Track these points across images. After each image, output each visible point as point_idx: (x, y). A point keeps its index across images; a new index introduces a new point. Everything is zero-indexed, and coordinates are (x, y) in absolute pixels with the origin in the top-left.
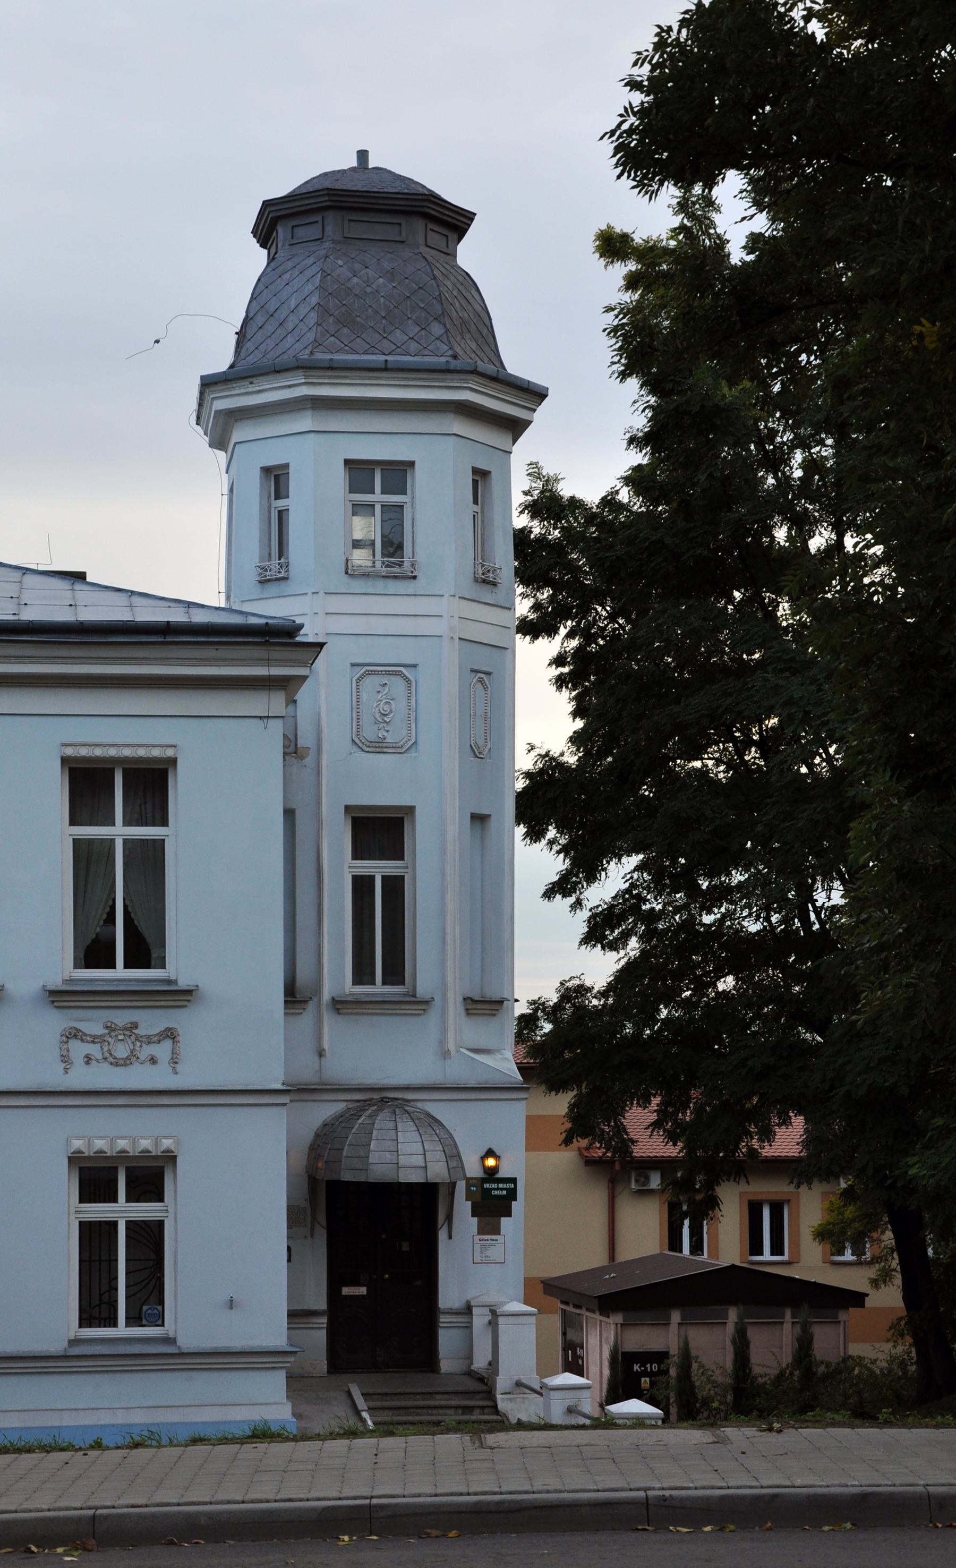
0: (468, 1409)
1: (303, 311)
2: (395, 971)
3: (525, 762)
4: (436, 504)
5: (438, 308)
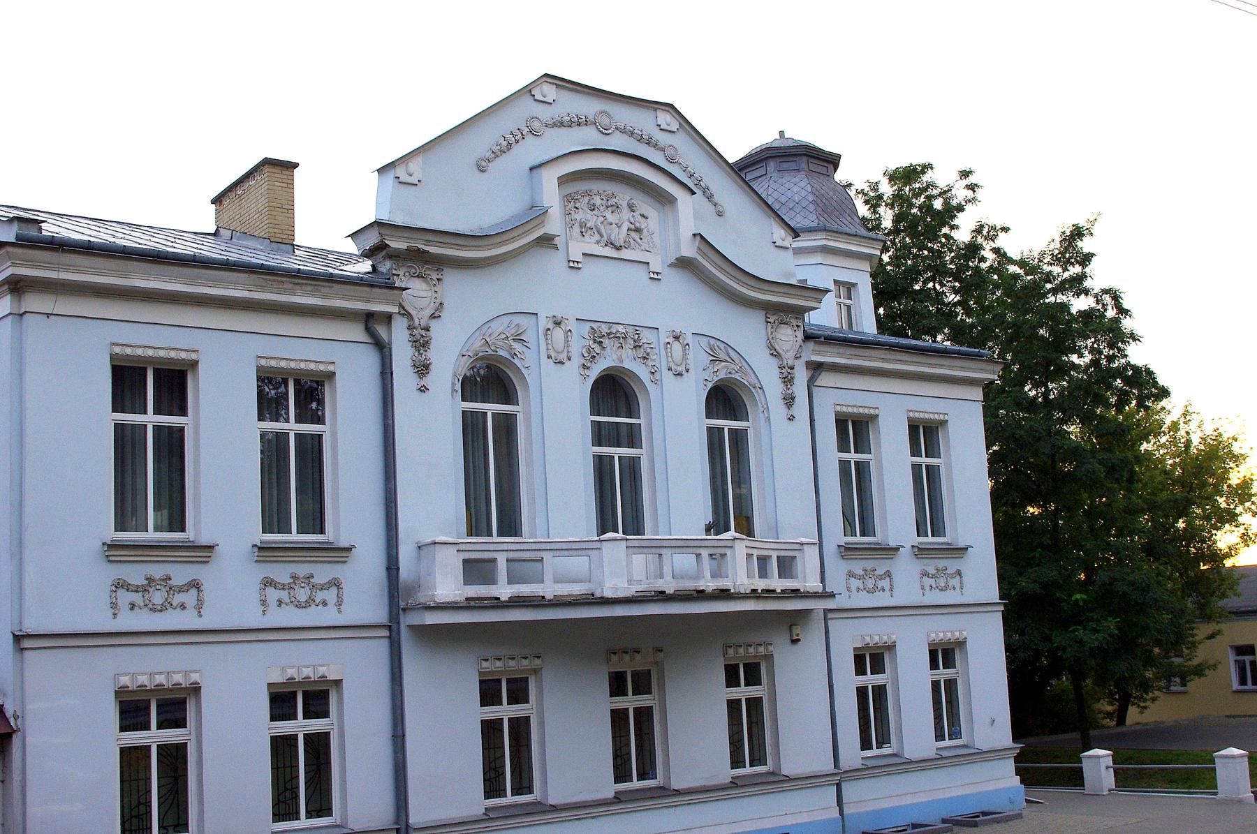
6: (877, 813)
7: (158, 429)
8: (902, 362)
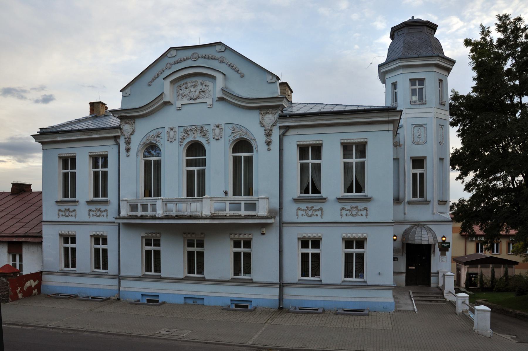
0: (437, 297)
2: (422, 195)
3: (452, 151)
4: (430, 89)
6: (301, 301)
7: (356, 163)
8: (330, 119)
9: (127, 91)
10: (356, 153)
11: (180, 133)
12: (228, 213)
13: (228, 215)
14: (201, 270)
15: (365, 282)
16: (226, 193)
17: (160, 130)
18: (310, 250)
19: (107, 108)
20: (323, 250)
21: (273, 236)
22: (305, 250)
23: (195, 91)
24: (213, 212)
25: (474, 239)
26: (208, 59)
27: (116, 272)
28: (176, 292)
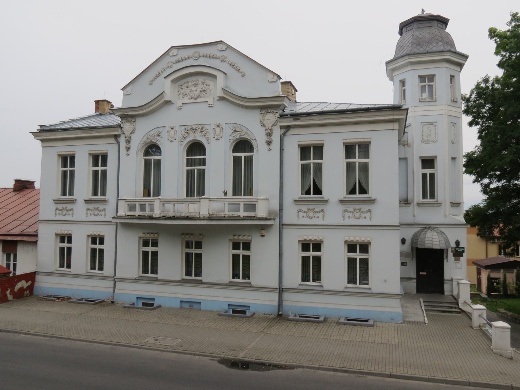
0: (451, 307)
1: (408, 45)
2: (432, 196)
5: (441, 39)
9: (129, 89)
10: (359, 152)
11: (181, 132)
12: (227, 213)
13: (226, 216)
14: (198, 273)
15: (370, 289)
16: (226, 194)
17: (160, 130)
18: (311, 254)
19: (112, 106)
20: (325, 254)
21: (273, 237)
22: (306, 254)
23: (196, 91)
24: (211, 213)
25: (496, 241)
26: (210, 57)
27: (112, 274)
28: (173, 295)
